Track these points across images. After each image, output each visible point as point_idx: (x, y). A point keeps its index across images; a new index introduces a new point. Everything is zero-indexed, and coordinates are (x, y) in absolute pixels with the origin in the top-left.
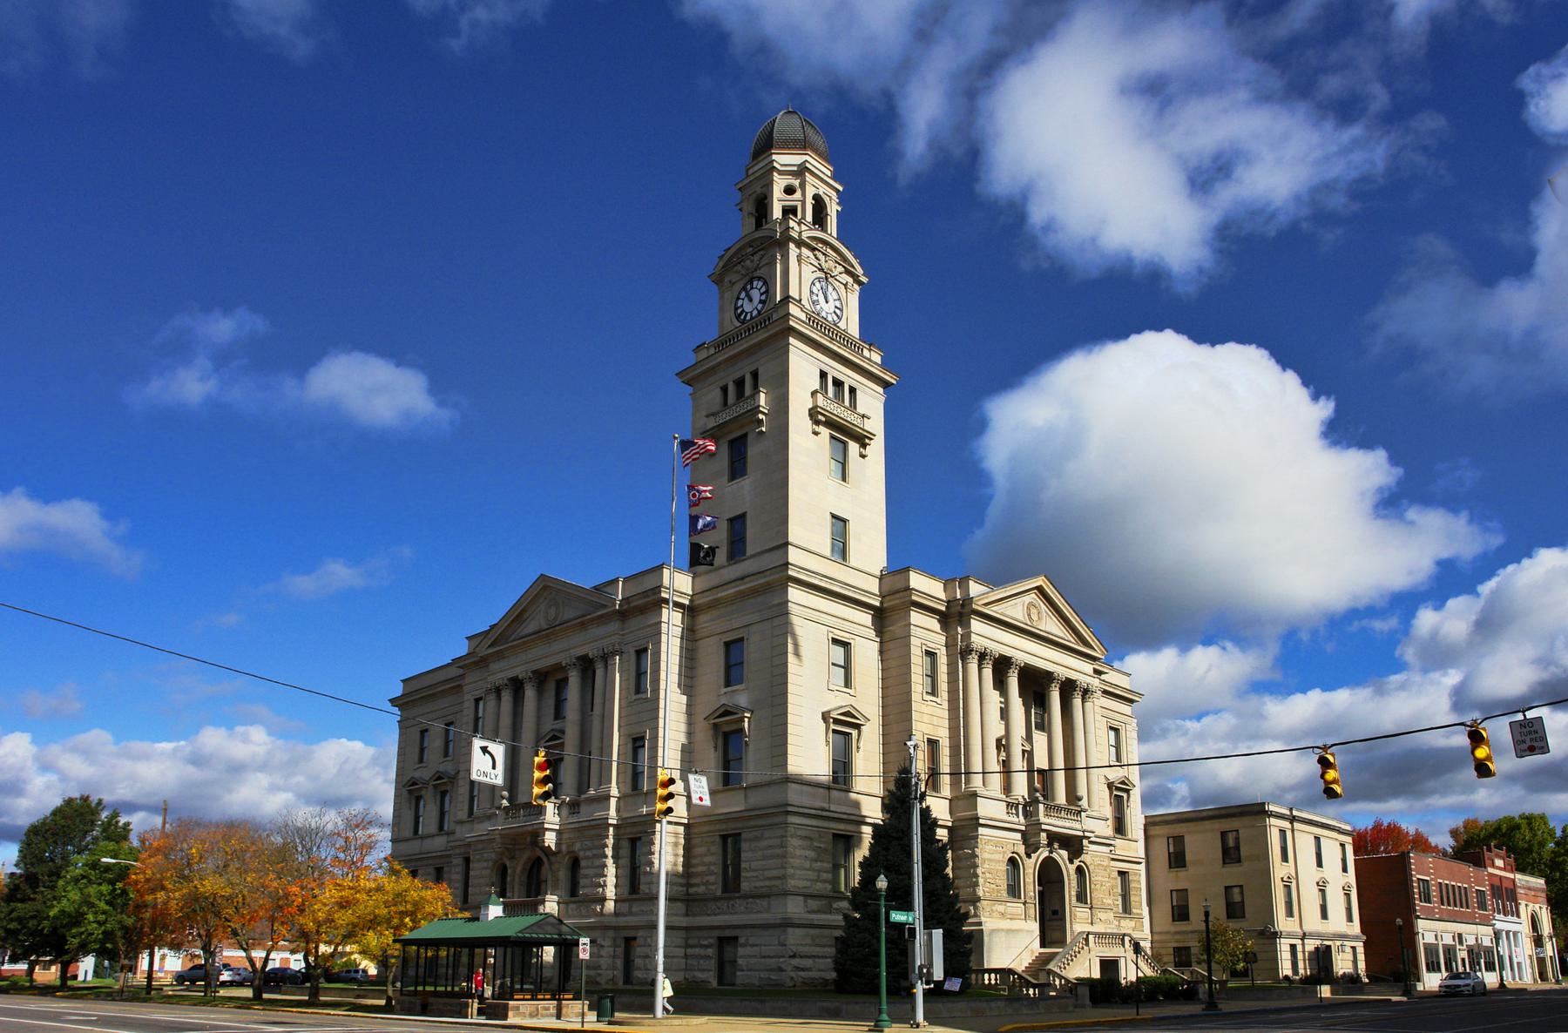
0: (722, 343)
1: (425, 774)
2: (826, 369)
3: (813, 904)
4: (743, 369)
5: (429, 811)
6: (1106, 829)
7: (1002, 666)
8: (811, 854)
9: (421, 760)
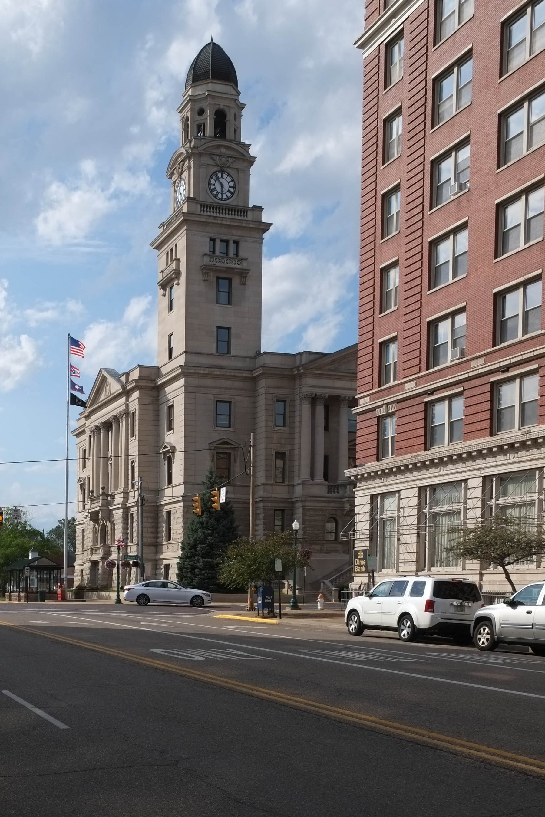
2: (212, 235)
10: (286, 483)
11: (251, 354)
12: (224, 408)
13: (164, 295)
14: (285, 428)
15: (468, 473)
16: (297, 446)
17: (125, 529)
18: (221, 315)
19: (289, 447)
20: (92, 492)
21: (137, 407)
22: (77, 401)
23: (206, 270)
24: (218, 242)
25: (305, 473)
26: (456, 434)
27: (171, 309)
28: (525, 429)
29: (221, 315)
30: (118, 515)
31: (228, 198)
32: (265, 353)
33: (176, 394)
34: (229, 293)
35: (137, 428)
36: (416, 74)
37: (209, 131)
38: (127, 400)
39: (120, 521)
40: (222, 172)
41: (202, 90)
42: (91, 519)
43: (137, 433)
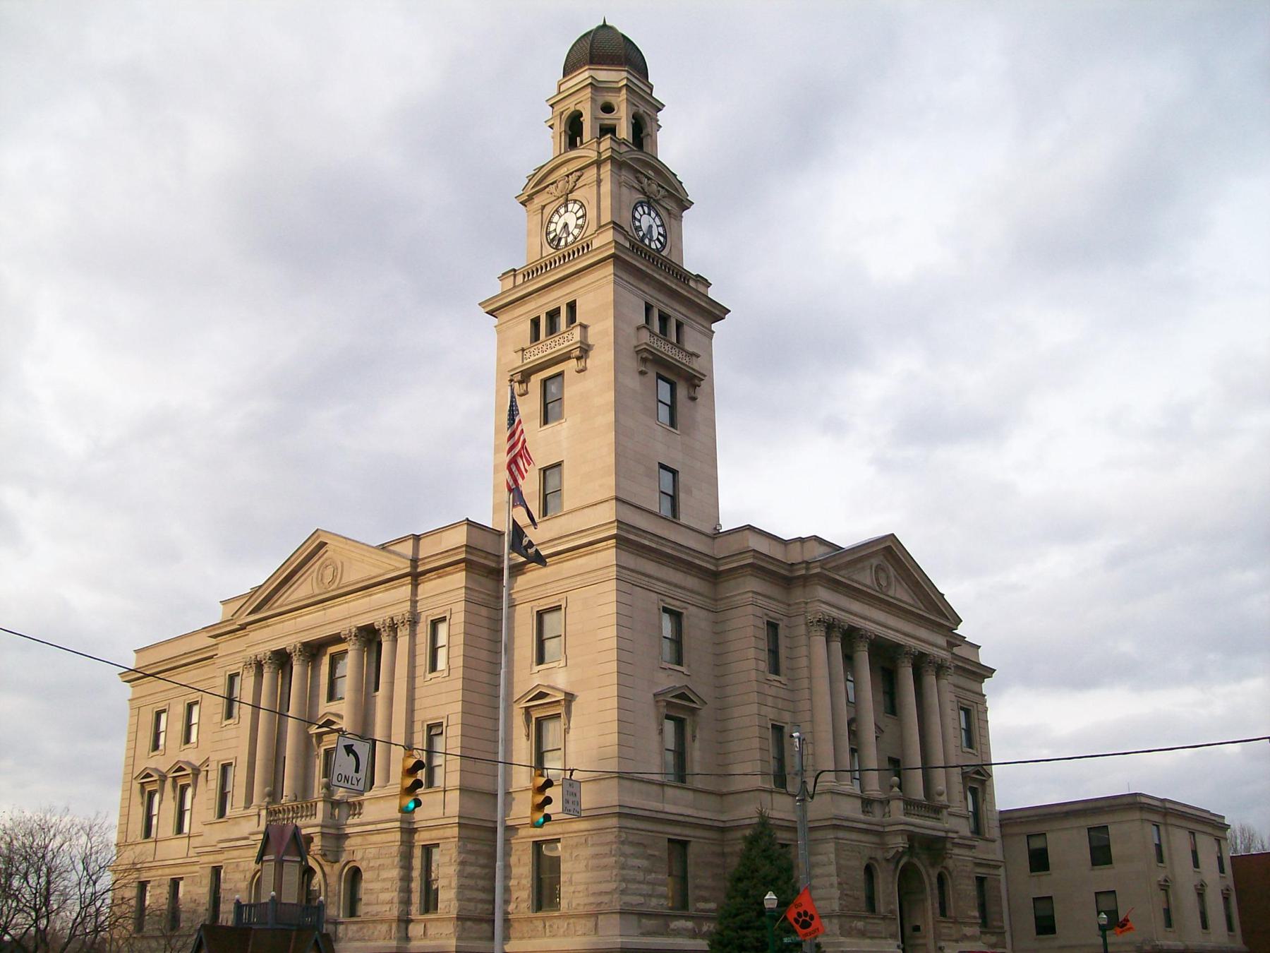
0: (531, 272)
1: (162, 763)
2: (653, 302)
3: (649, 923)
4: (557, 299)
5: (165, 808)
6: (965, 828)
7: (850, 637)
8: (644, 863)
9: (156, 747)
18: (665, 447)
22: (525, 542)
37: (624, 131)
38: (414, 592)
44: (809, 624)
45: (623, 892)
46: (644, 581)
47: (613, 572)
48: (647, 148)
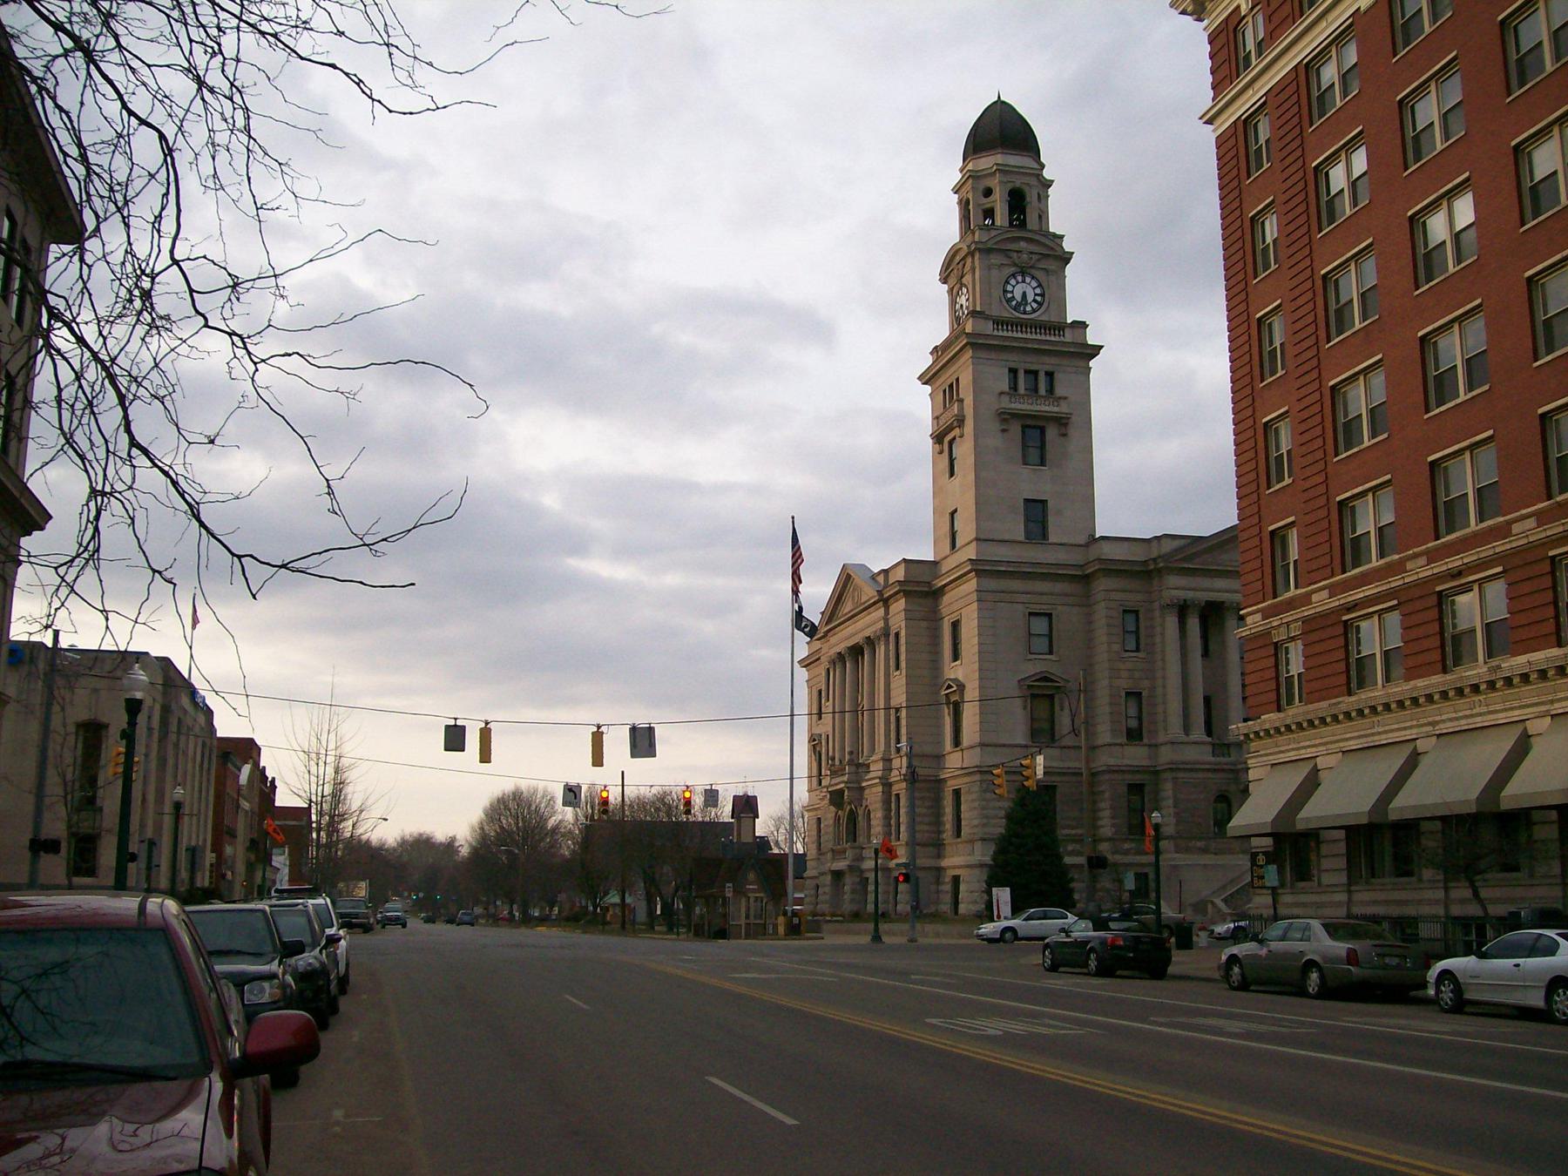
2: (1013, 365)
10: (1145, 741)
11: (1082, 540)
12: (1040, 626)
13: (941, 452)
14: (1141, 655)
15: (1415, 731)
16: (1159, 682)
17: (887, 817)
18: (1032, 482)
19: (1146, 683)
20: (833, 759)
21: (903, 624)
23: (1006, 417)
24: (1021, 375)
25: (1175, 721)
26: (1393, 675)
27: (952, 474)
28: (1494, 662)
29: (1032, 482)
30: (874, 796)
31: (1034, 311)
32: (1103, 538)
33: (963, 604)
34: (1042, 447)
35: (903, 657)
36: (1290, 159)
37: (1001, 217)
38: (887, 612)
39: (879, 805)
40: (1023, 274)
41: (986, 162)
42: (832, 802)
43: (903, 665)
44: (1162, 607)
45: (984, 825)
46: (1007, 597)
47: (974, 596)
48: (1032, 222)
